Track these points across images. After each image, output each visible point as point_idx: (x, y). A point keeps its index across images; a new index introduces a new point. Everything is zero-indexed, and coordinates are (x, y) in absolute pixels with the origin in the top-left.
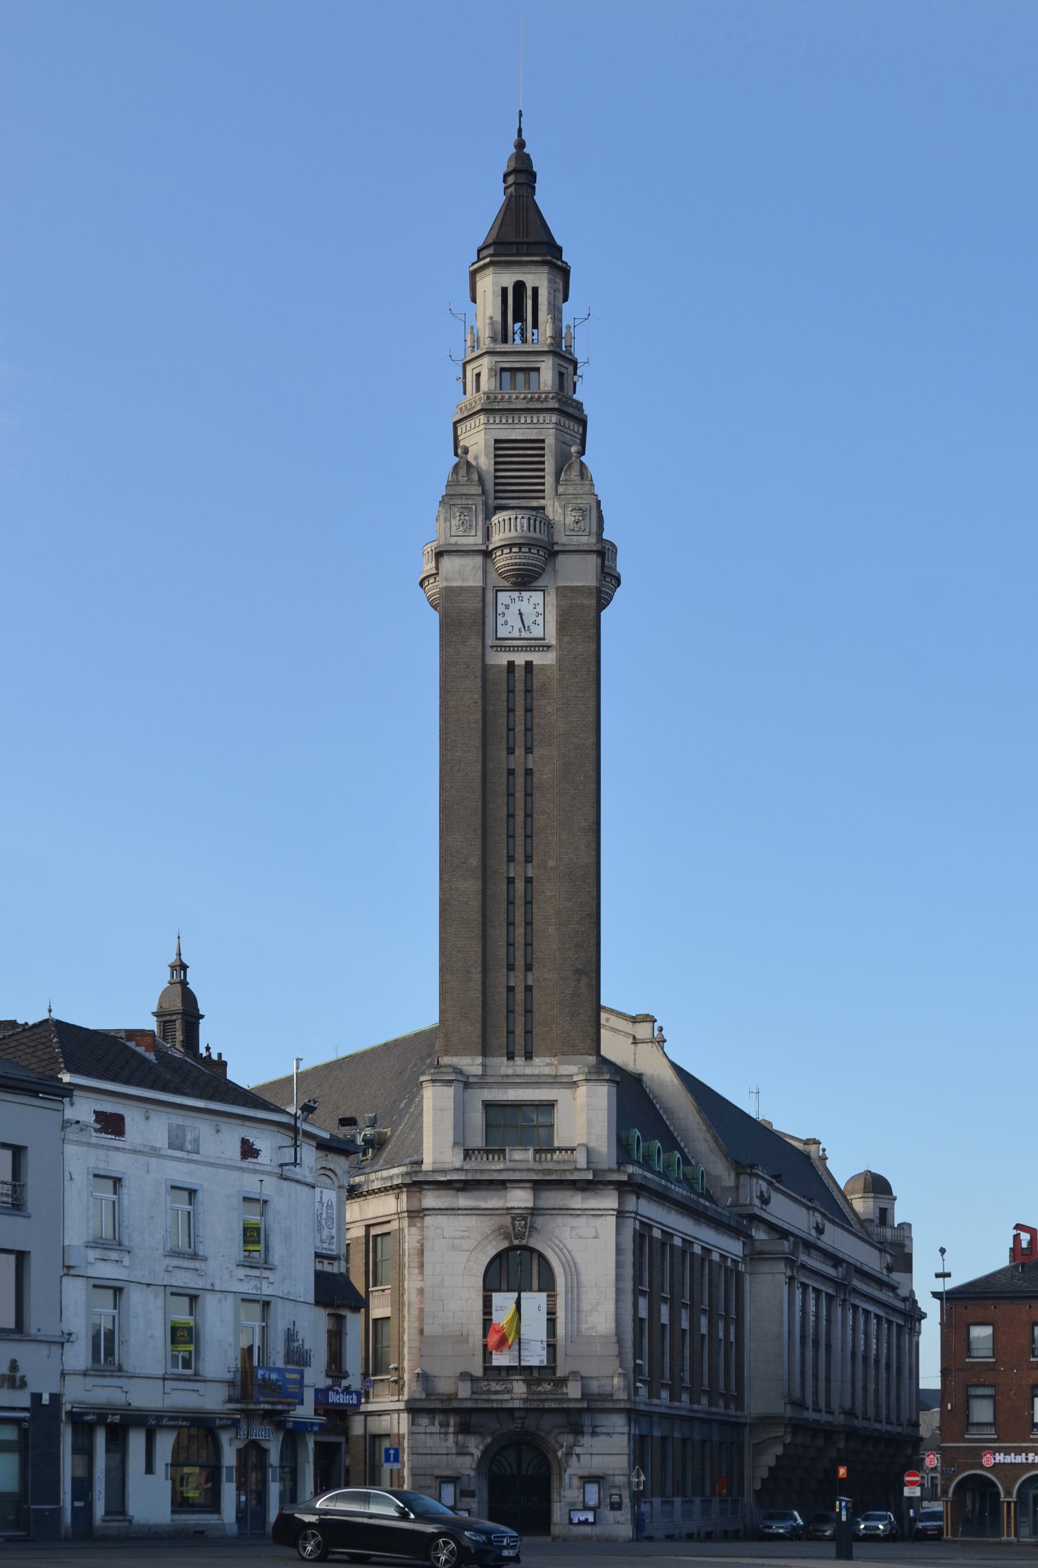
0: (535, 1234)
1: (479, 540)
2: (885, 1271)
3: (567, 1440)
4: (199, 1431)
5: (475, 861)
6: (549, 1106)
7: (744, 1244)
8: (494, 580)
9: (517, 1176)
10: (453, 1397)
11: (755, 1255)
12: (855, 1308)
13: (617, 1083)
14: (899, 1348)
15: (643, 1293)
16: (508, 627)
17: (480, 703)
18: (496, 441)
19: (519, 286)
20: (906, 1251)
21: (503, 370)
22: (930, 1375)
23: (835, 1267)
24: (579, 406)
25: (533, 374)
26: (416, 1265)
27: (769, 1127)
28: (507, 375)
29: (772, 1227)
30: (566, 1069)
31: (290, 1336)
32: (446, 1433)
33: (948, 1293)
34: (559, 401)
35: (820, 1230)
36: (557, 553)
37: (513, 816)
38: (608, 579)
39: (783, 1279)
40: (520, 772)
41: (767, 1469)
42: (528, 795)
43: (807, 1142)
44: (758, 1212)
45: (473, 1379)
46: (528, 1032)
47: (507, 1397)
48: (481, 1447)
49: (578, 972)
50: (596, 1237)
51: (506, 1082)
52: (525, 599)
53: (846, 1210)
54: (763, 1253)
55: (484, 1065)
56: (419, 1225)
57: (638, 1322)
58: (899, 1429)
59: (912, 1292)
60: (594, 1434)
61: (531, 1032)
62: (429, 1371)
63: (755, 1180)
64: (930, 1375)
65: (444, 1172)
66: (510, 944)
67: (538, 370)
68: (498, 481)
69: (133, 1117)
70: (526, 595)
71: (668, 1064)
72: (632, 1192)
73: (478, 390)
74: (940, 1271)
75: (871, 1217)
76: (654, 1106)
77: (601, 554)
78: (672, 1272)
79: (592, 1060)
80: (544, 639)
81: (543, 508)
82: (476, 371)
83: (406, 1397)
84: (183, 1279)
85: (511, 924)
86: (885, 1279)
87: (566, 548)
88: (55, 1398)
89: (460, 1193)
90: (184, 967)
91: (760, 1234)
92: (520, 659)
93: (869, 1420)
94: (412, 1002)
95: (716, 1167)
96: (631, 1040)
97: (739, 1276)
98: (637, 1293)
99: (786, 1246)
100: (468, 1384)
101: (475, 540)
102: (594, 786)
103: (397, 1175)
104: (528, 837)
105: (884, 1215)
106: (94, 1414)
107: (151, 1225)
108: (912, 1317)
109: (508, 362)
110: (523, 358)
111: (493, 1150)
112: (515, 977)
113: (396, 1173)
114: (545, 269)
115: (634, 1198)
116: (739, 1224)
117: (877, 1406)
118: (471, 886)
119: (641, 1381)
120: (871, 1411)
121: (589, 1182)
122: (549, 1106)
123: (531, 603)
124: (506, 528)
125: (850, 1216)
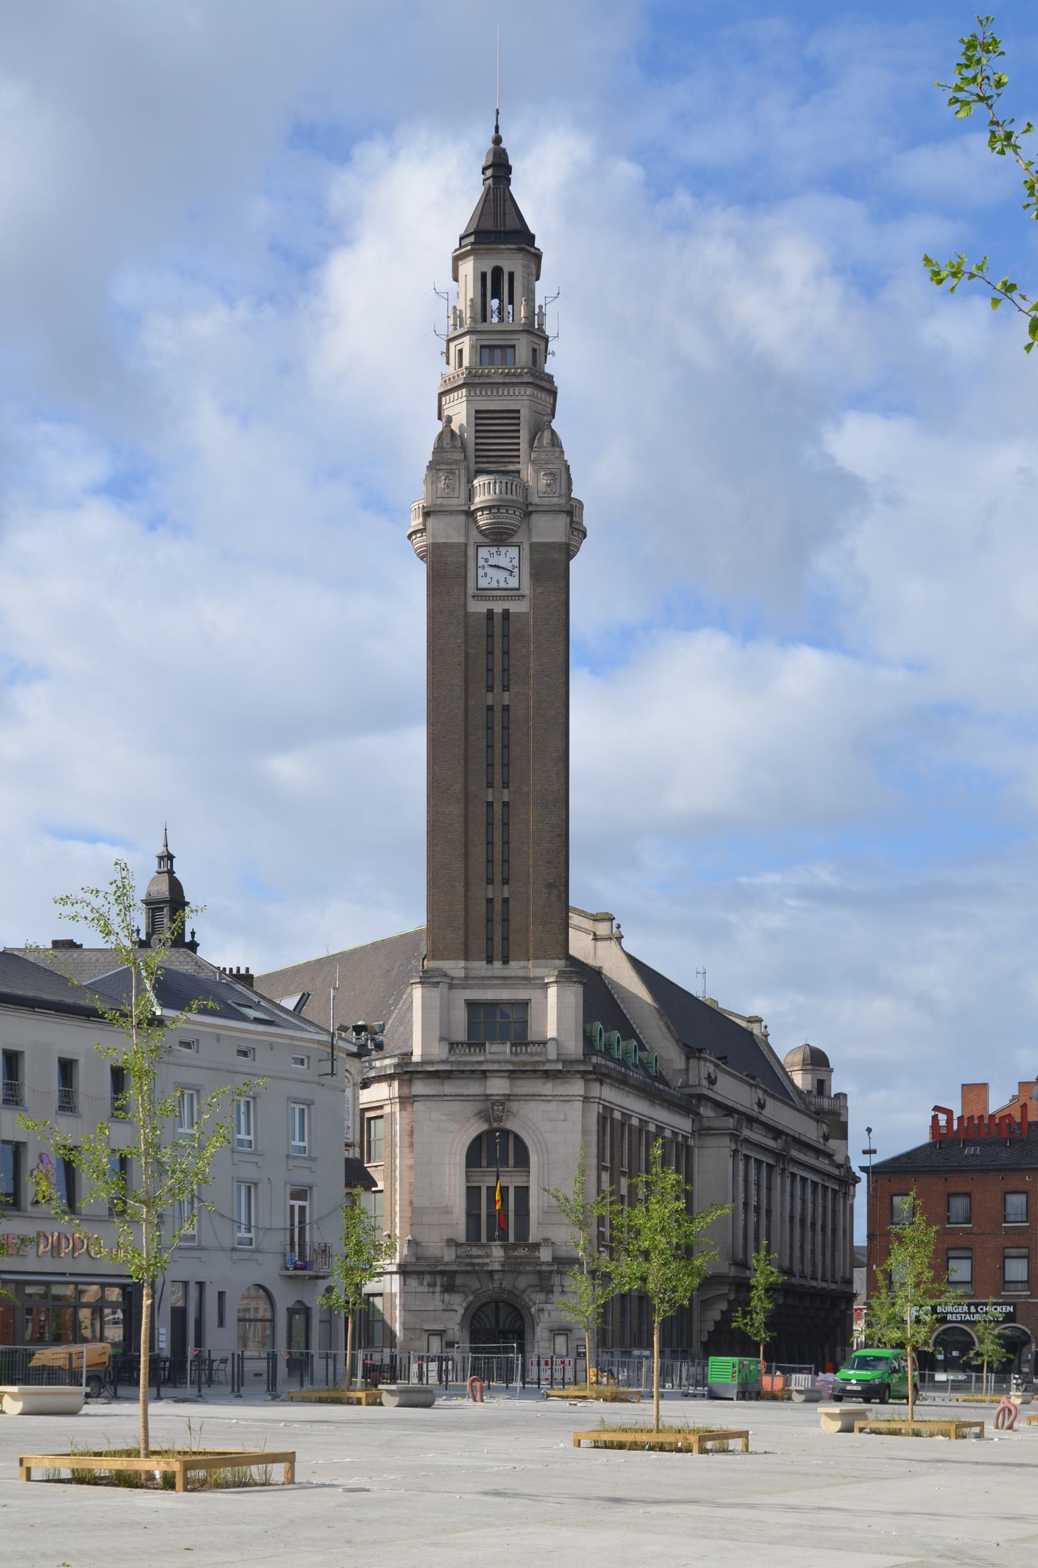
0: (511, 1118)
1: (462, 500)
2: (821, 1140)
3: (540, 1297)
5: (458, 788)
6: (525, 1004)
7: (693, 1121)
8: (475, 536)
9: (496, 1067)
10: (439, 1260)
11: (702, 1131)
12: (793, 1175)
13: (584, 984)
14: (834, 1211)
15: (605, 1168)
17: (463, 647)
18: (477, 412)
19: (497, 272)
20: (842, 1119)
21: (482, 347)
22: (860, 1237)
23: (775, 1139)
24: (550, 378)
25: (509, 351)
26: (407, 1144)
27: (713, 1006)
28: (486, 351)
29: (718, 1105)
32: (433, 1293)
33: (874, 1167)
34: (533, 375)
35: (761, 1106)
36: (530, 513)
37: (492, 747)
38: (575, 533)
39: (728, 1152)
40: (498, 709)
41: (712, 1323)
42: (506, 728)
43: (750, 1020)
44: (706, 1092)
45: (458, 1245)
46: (505, 939)
47: (487, 1260)
48: (464, 1305)
49: (550, 886)
50: (565, 1120)
51: (485, 982)
52: (503, 553)
53: (786, 1083)
54: (710, 1128)
55: (465, 968)
56: (409, 1109)
58: (833, 1286)
59: (847, 1158)
60: (563, 1292)
61: (508, 939)
62: (419, 1239)
63: (702, 1063)
64: (860, 1237)
65: (432, 1063)
66: (490, 861)
67: (514, 347)
68: (478, 447)
70: (503, 550)
71: (625, 958)
72: (596, 1080)
73: (461, 365)
74: (867, 1148)
75: (810, 1088)
76: (612, 996)
77: (570, 513)
78: (630, 1149)
79: (561, 963)
80: (519, 589)
81: (518, 472)
82: (459, 347)
83: (397, 1261)
85: (490, 843)
86: (822, 1147)
87: (540, 509)
89: (446, 1082)
90: (170, 857)
91: (706, 1111)
92: (498, 607)
93: (806, 1278)
94: (394, 906)
95: (668, 1052)
96: (591, 937)
97: (689, 1150)
98: (601, 1168)
99: (730, 1122)
100: (453, 1249)
101: (458, 501)
102: (563, 720)
103: (390, 1066)
104: (506, 765)
105: (821, 1086)
108: (846, 1182)
110: (500, 337)
111: (475, 1041)
112: (494, 890)
113: (386, 1064)
114: (521, 255)
115: (598, 1085)
116: (687, 1103)
117: (814, 1265)
118: (456, 810)
119: (603, 1246)
120: (808, 1270)
121: (560, 1071)
122: (525, 1004)
123: (508, 556)
124: (485, 491)
125: (790, 1089)
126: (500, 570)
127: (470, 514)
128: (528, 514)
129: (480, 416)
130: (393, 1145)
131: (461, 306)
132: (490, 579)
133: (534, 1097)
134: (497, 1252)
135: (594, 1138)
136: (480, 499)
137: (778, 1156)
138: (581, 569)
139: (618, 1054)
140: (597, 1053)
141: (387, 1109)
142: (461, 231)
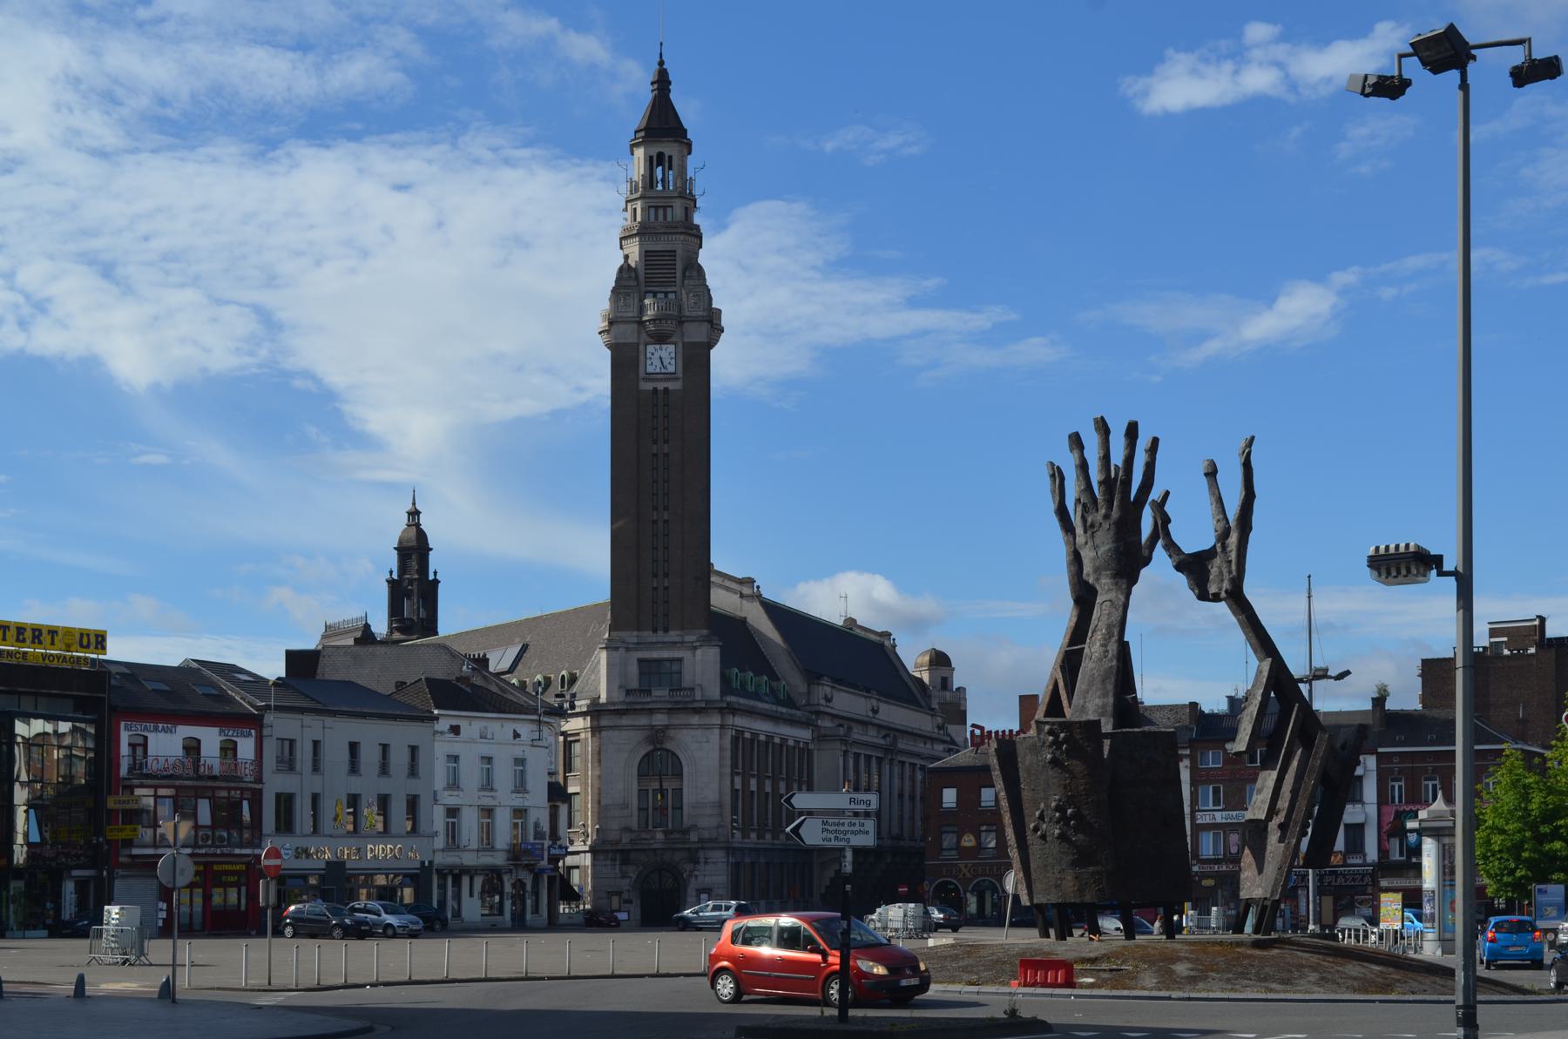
4: (493, 877)
11: (821, 737)
16: (653, 366)
30: (688, 638)
31: (537, 825)
35: (875, 711)
57: (734, 792)
69: (463, 724)
77: (710, 322)
84: (487, 802)
88: (431, 862)
92: (661, 386)
95: (792, 678)
97: (810, 752)
98: (733, 774)
105: (945, 683)
106: (1082, 986)
107: (471, 774)
109: (654, 202)
126: (661, 359)
127: (641, 323)
128: (681, 323)
129: (647, 255)
130: (586, 761)
131: (635, 178)
132: (653, 366)
133: (687, 726)
134: (660, 836)
135: (728, 754)
136: (650, 314)
137: (886, 750)
138: (719, 356)
139: (751, 688)
140: (733, 692)
141: (582, 736)
142: (635, 127)
